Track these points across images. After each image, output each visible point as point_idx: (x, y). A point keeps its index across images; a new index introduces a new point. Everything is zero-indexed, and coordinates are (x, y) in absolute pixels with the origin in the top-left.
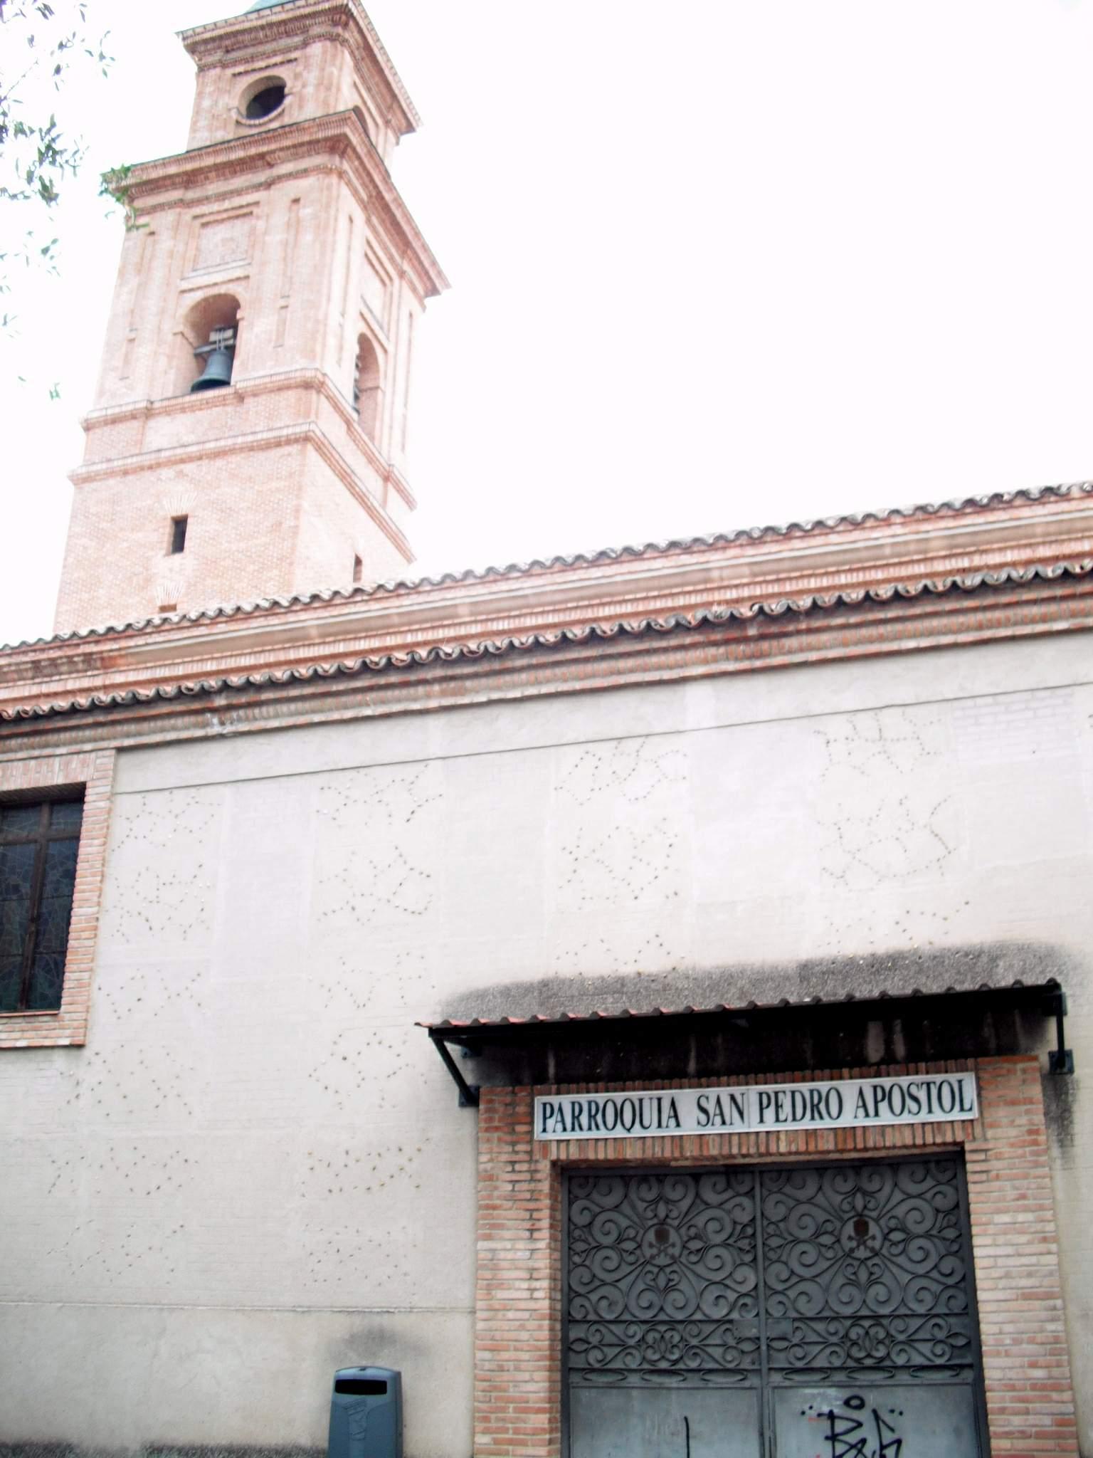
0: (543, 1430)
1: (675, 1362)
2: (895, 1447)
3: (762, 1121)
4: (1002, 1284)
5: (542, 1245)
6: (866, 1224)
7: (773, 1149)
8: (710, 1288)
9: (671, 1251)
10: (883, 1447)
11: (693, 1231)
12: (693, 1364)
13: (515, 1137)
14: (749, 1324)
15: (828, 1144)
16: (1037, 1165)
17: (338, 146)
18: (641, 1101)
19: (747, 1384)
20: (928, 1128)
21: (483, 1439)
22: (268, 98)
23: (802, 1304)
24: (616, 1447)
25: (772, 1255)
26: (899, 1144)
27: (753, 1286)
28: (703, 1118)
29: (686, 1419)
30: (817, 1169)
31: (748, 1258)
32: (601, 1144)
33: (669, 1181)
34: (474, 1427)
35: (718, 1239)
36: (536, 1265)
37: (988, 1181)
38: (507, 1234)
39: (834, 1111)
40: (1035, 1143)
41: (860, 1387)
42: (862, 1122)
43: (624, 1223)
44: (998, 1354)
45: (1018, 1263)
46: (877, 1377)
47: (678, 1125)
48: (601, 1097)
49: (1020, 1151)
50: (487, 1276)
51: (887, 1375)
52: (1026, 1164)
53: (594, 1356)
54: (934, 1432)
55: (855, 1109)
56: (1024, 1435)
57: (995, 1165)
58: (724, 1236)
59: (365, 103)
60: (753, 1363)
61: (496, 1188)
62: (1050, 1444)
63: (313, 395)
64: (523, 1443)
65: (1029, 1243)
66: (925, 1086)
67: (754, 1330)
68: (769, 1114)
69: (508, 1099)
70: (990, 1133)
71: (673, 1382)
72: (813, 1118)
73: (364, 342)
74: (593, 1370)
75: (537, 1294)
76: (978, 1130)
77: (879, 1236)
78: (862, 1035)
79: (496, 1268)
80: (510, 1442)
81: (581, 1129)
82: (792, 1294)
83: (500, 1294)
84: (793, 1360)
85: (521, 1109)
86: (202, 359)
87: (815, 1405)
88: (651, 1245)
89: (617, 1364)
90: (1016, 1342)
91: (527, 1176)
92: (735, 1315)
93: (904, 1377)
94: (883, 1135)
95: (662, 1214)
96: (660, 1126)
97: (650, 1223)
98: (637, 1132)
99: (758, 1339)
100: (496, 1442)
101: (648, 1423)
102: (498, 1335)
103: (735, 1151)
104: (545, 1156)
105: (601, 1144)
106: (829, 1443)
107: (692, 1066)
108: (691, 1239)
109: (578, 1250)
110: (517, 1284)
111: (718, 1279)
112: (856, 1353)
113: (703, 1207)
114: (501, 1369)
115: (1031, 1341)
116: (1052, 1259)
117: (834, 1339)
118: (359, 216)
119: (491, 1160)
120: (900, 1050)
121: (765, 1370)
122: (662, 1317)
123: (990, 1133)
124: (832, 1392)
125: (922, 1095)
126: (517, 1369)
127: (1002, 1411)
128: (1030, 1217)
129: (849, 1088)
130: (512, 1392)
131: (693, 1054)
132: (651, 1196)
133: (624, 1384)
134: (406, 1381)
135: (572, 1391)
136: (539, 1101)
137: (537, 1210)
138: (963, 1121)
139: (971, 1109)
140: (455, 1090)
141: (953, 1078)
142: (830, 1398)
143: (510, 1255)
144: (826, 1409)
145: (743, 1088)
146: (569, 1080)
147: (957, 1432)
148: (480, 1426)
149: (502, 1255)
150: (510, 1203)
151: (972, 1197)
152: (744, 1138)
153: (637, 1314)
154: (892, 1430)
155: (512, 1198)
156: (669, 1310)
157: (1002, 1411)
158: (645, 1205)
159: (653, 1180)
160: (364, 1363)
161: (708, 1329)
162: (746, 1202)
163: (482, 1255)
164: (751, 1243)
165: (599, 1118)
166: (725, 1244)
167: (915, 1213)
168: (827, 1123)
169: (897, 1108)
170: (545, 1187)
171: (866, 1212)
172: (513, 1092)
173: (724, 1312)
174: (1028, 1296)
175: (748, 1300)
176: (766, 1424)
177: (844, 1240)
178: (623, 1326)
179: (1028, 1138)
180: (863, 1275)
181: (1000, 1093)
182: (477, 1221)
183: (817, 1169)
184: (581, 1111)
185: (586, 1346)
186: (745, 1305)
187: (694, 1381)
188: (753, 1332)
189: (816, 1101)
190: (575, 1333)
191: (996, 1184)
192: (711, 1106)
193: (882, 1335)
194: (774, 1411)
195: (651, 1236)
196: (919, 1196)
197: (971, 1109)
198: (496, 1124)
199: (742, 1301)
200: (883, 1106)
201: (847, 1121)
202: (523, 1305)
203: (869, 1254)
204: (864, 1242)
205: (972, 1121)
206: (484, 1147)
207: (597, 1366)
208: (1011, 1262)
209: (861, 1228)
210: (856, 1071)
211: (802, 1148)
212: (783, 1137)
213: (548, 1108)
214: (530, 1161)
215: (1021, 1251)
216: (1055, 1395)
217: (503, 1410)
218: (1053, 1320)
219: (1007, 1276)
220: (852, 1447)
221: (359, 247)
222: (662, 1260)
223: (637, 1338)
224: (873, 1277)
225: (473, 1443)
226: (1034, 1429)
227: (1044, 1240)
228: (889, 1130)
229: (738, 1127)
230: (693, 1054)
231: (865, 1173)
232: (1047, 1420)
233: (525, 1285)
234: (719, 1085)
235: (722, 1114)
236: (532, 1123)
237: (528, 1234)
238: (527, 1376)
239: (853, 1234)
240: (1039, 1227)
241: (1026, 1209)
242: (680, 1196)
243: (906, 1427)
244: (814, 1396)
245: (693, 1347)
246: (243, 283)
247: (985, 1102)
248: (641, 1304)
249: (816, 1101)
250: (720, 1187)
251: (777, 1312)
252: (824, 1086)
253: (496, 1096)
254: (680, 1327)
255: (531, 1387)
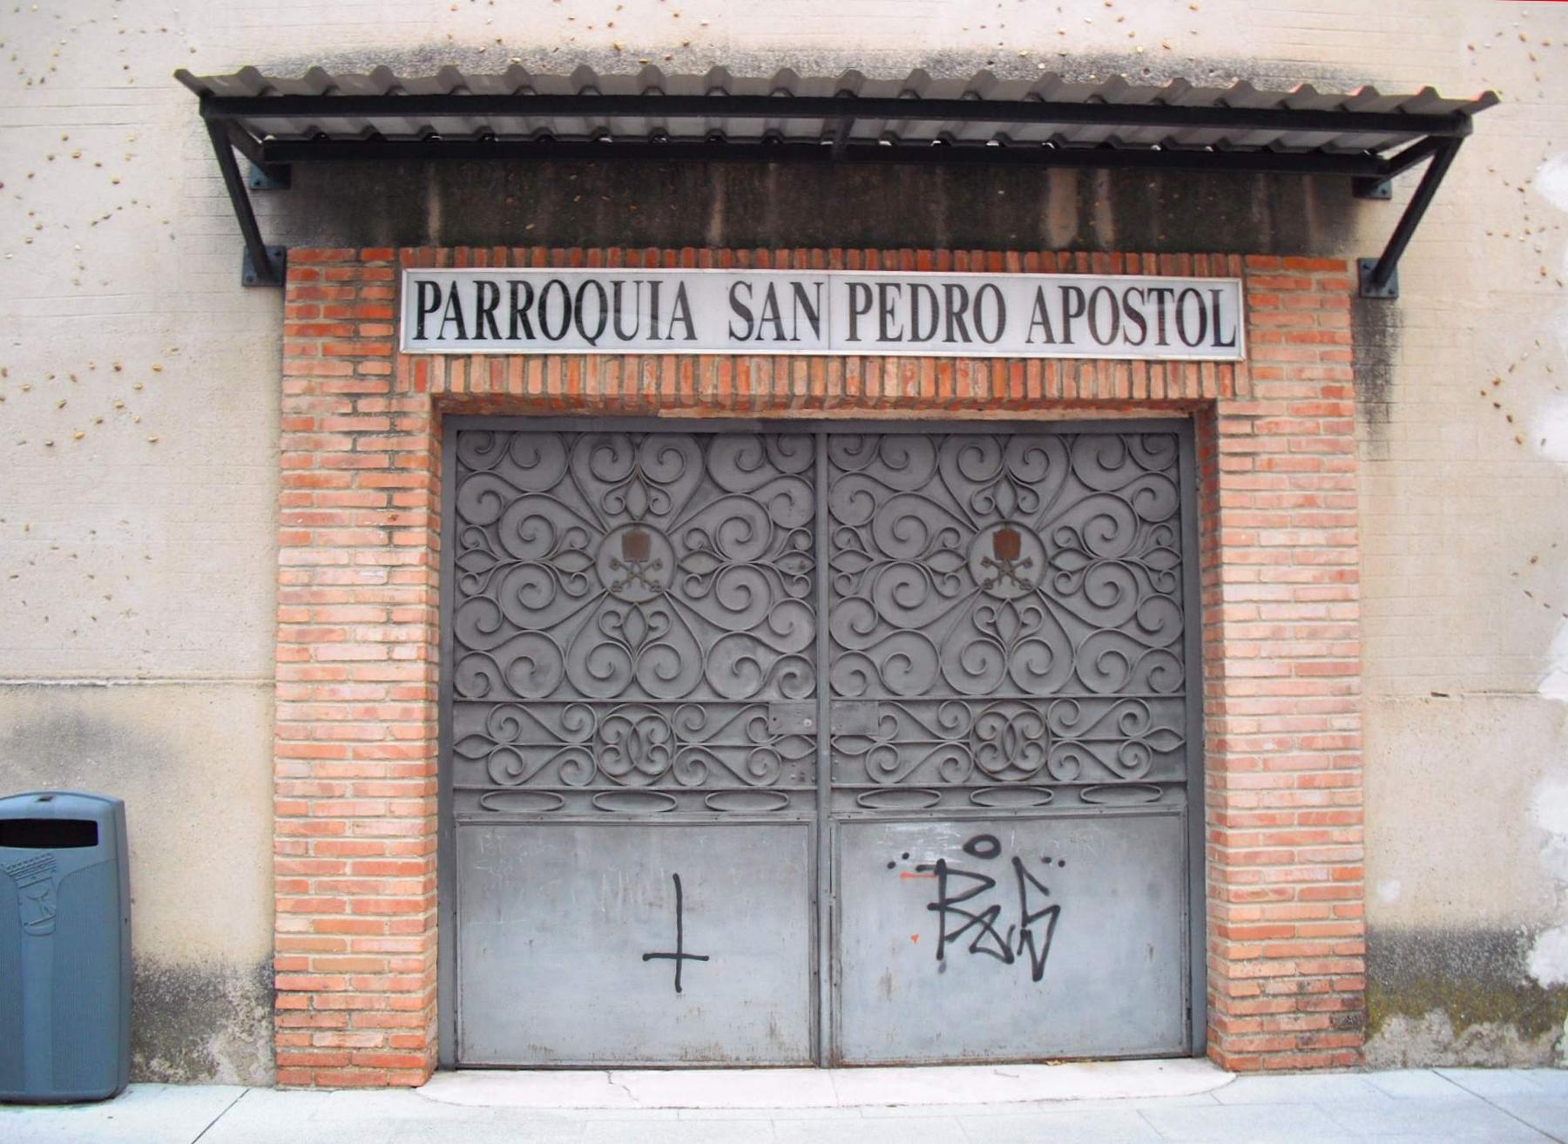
0: (414, 907)
1: (658, 778)
2: (1047, 919)
3: (853, 336)
4: (1267, 648)
5: (413, 556)
6: (1016, 539)
7: (873, 389)
8: (728, 650)
9: (651, 575)
10: (1027, 919)
11: (695, 541)
12: (692, 782)
13: (358, 348)
14: (797, 712)
15: (976, 387)
16: (1336, 449)
18: (618, 285)
19: (791, 815)
20: (1157, 370)
21: (292, 924)
23: (896, 677)
24: (542, 928)
25: (842, 587)
26: (1104, 395)
27: (807, 642)
28: (741, 327)
29: (676, 878)
30: (930, 436)
31: (798, 592)
32: (535, 365)
33: (651, 446)
34: (275, 901)
35: (742, 556)
36: (399, 596)
37: (1254, 471)
38: (340, 535)
39: (990, 327)
40: (1335, 411)
41: (994, 820)
42: (1039, 349)
43: (563, 520)
44: (1251, 766)
45: (1295, 615)
46: (1025, 803)
47: (691, 335)
48: (538, 276)
49: (1309, 424)
50: (298, 618)
51: (668, 806)
52: (1321, 448)
53: (501, 766)
54: (1114, 892)
55: (1039, 326)
56: (1282, 895)
57: (1266, 443)
58: (754, 550)
60: (802, 780)
61: (318, 445)
62: (1322, 907)
64: (376, 930)
65: (1317, 580)
66: (1154, 295)
67: (808, 722)
68: (869, 324)
69: (347, 272)
70: (1261, 388)
71: (651, 812)
72: (950, 339)
74: (501, 793)
75: (400, 652)
76: (1241, 382)
77: (1037, 560)
78: (1038, 194)
79: (318, 600)
80: (347, 928)
81: (496, 335)
82: (502, 658)
83: (328, 651)
84: (875, 774)
85: (374, 292)
87: (913, 852)
88: (615, 564)
89: (548, 782)
90: (1283, 745)
91: (384, 424)
92: (771, 695)
93: (1069, 804)
94: (1076, 377)
95: (637, 507)
96: (654, 335)
97: (614, 523)
98: (609, 344)
99: (814, 737)
100: (320, 928)
101: (605, 887)
102: (320, 729)
103: (800, 389)
104: (420, 385)
105: (535, 365)
106: (936, 914)
107: (716, 229)
108: (691, 553)
109: (847, 570)
110: (361, 631)
111: (1109, 626)
112: (992, 763)
113: (715, 495)
114: (328, 793)
115: (1307, 745)
116: (1349, 610)
117: (952, 739)
119: (309, 391)
120: (1105, 229)
121: (824, 792)
122: (635, 696)
123: (1261, 388)
124: (945, 829)
125: (1149, 310)
126: (359, 793)
127: (1251, 858)
128: (1319, 536)
129: (1019, 287)
130: (349, 836)
131: (718, 206)
132: (616, 472)
133: (559, 817)
134: (132, 816)
135: (459, 830)
136: (410, 278)
137: (404, 489)
138: (1217, 363)
139: (1232, 344)
140: (237, 246)
141: (1204, 285)
142: (940, 840)
143: (346, 576)
144: (931, 859)
145: (819, 274)
147: (1153, 890)
148: (287, 900)
149: (330, 575)
150: (347, 475)
151: (1225, 497)
152: (818, 367)
153: (586, 690)
154: (1044, 890)
155: (352, 464)
156: (648, 683)
157: (1251, 858)
158: (606, 488)
159: (620, 443)
160: (45, 786)
161: (719, 718)
162: (798, 490)
163: (287, 577)
164: (802, 566)
165: (968, 318)
166: (756, 567)
167: (1105, 523)
168: (978, 349)
169: (1104, 329)
170: (420, 444)
171: (650, 520)
172: (358, 260)
173: (750, 690)
174: (1308, 670)
175: (796, 668)
176: (824, 886)
177: (976, 568)
178: (556, 713)
179: (1325, 402)
180: (634, 630)
181: (1282, 319)
182: (277, 512)
183: (930, 436)
184: (495, 303)
185: (486, 749)
186: (792, 675)
187: (691, 811)
188: (807, 725)
189: (956, 307)
190: (468, 723)
191: (1266, 478)
192: (757, 305)
193: (660, 737)
194: (839, 863)
195: (615, 547)
196: (747, 496)
197: (1232, 344)
198: (321, 320)
199: (785, 670)
200: (1080, 326)
201: (1013, 345)
202: (372, 672)
203: (647, 594)
204: (641, 575)
205: (1232, 364)
206: (293, 364)
207: (508, 784)
208: (1287, 611)
209: (1007, 545)
210: (1031, 257)
211: (928, 391)
212: (891, 367)
213: (429, 290)
214: (389, 395)
215: (1302, 595)
216: (1336, 833)
217: (335, 869)
218: (1346, 710)
219: (1277, 635)
220: (975, 920)
222: (635, 593)
223: (585, 735)
224: (653, 635)
225: (274, 930)
226: (1299, 887)
227: (1341, 577)
228: (1086, 369)
229: (809, 345)
230: (718, 206)
231: (1017, 446)
232: (1320, 872)
233: (377, 634)
234: (773, 266)
235: (776, 317)
236: (396, 320)
237: (383, 534)
238: (380, 806)
239: (991, 556)
240: (1333, 554)
241: (1313, 524)
242: (675, 474)
243: (1068, 888)
244: (912, 836)
245: (692, 750)
247: (1256, 333)
248: (595, 667)
249: (956, 307)
250: (748, 461)
251: (850, 689)
252: (971, 280)
253: (322, 264)
254: (666, 714)
255: (388, 827)
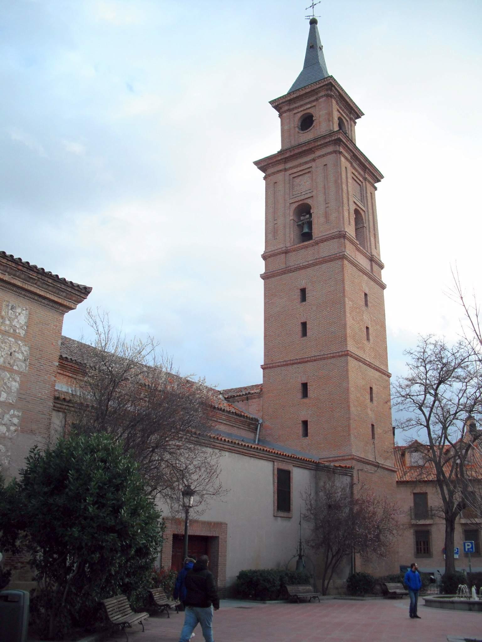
17: (338, 142)
22: (307, 122)
59: (342, 115)
63: (342, 240)
73: (357, 212)
86: (301, 227)
118: (348, 165)
131: (455, 506)
146: (230, 451)
221: (350, 175)
230: (455, 506)
246: (311, 199)
